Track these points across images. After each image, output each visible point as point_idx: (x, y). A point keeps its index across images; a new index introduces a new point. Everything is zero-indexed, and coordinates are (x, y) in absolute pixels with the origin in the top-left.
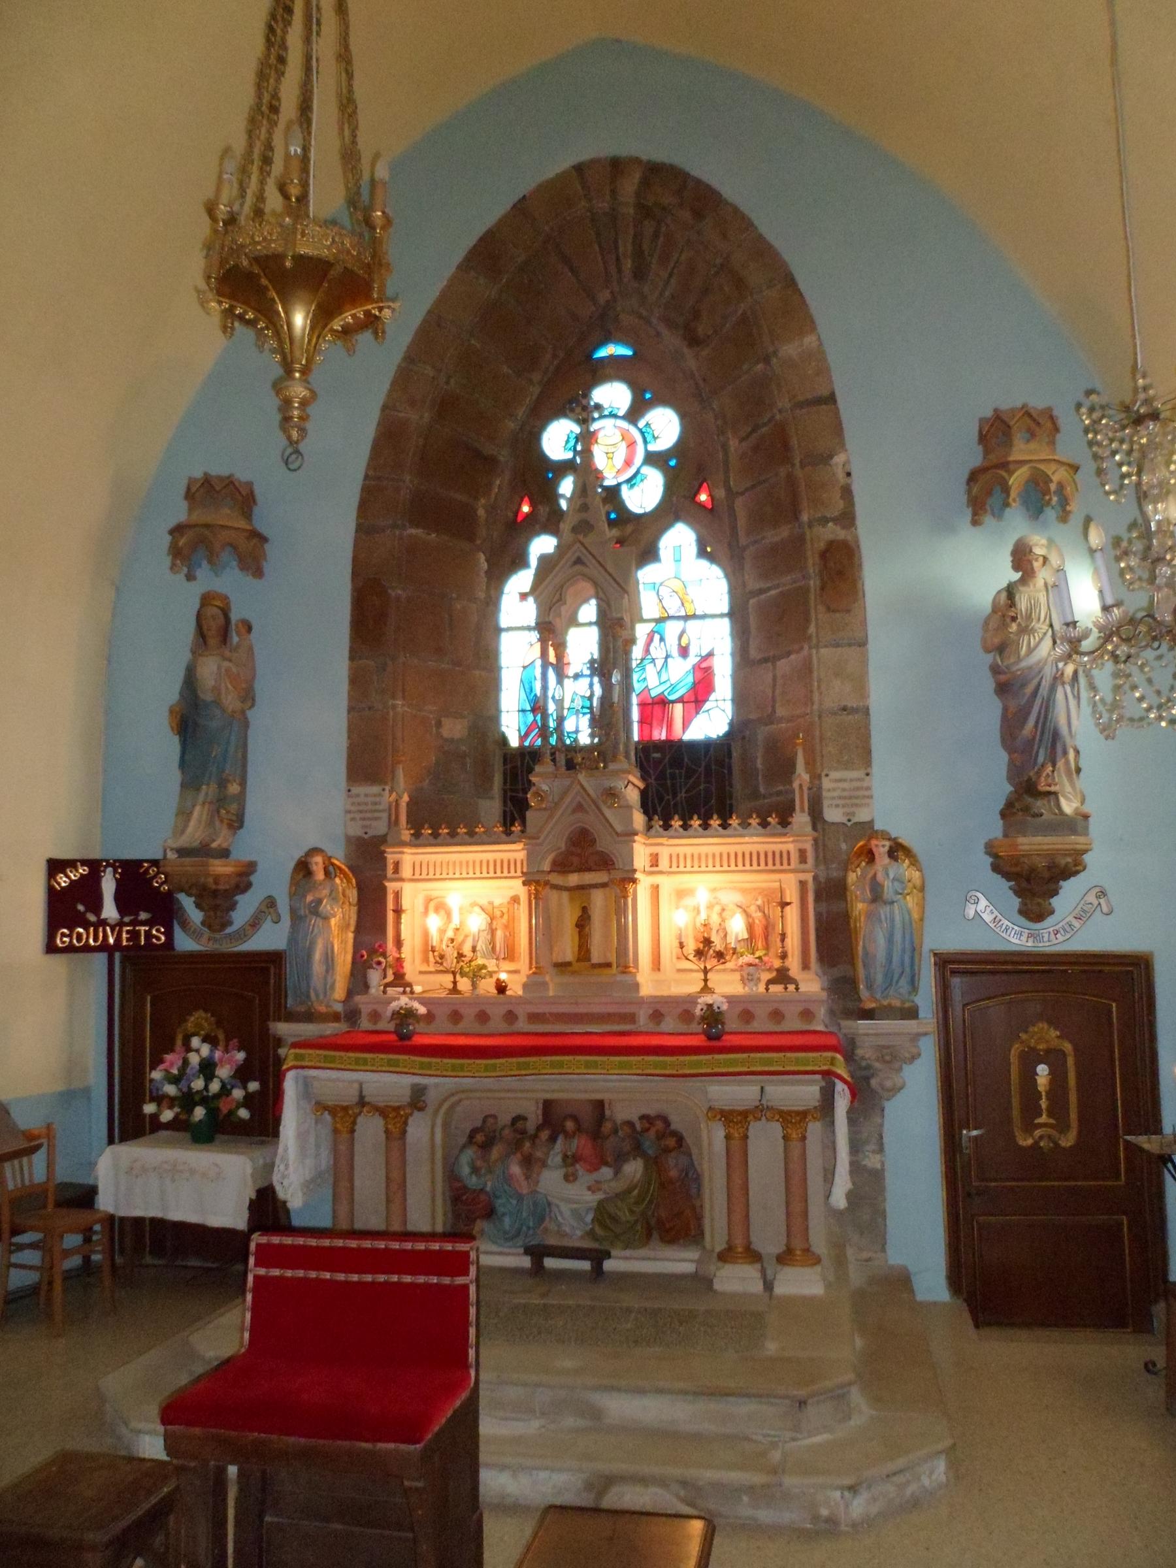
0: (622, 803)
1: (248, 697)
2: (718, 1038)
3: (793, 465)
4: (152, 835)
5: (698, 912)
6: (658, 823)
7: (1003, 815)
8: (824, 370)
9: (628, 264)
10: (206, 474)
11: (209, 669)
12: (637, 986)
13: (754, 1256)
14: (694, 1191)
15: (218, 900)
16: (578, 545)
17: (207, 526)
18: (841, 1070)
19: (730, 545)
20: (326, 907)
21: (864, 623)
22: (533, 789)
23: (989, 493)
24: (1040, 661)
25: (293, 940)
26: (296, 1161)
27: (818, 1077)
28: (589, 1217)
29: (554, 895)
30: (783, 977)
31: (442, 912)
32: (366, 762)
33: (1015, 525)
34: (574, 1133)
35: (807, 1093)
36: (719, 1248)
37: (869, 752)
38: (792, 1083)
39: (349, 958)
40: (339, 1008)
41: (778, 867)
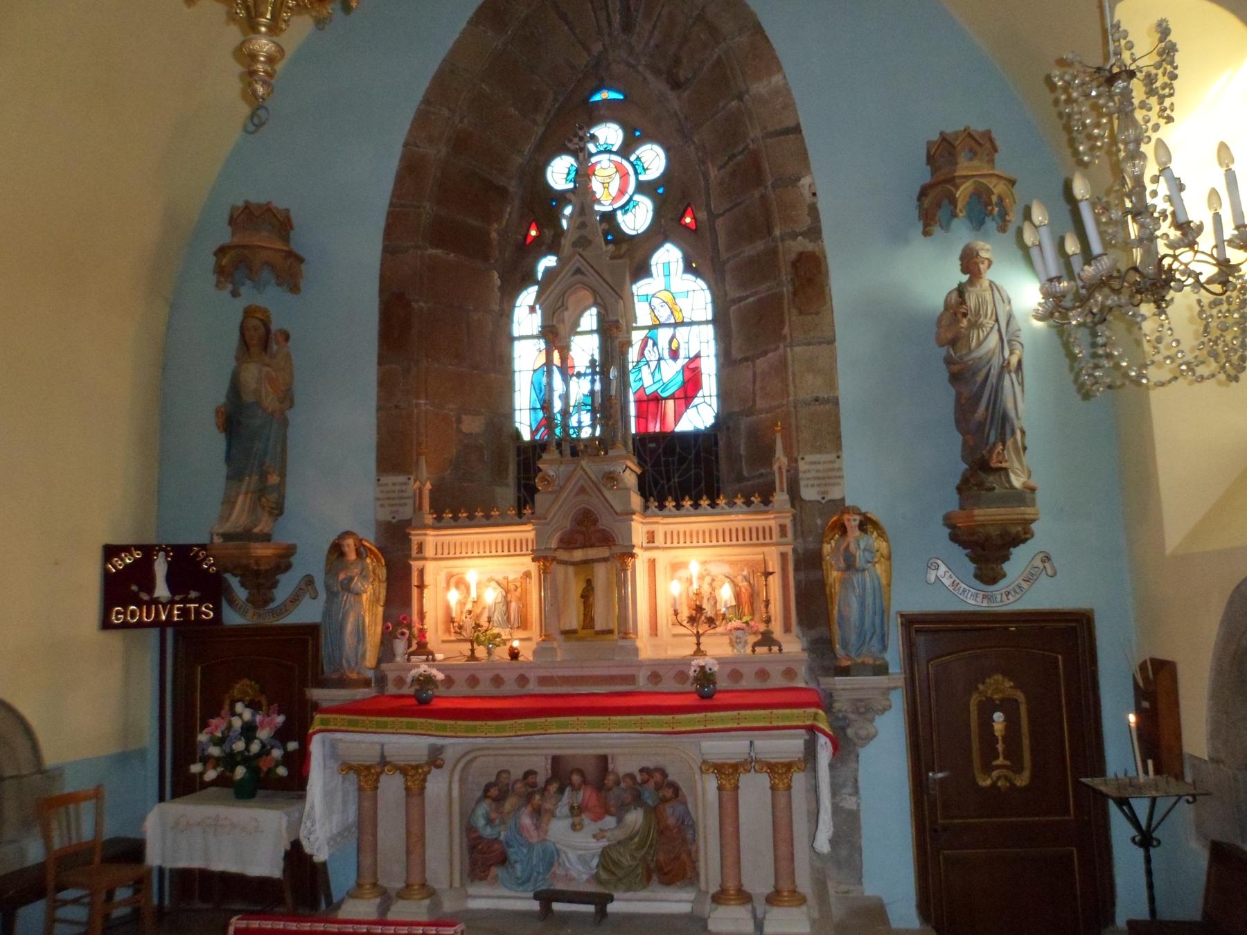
0: (621, 485)
1: (287, 398)
2: (710, 696)
3: (766, 188)
4: (200, 524)
5: (691, 583)
6: (653, 504)
7: (959, 489)
8: (789, 105)
9: (617, 19)
10: (246, 202)
11: (251, 373)
12: (636, 650)
13: (744, 897)
14: (689, 836)
15: (262, 579)
16: (578, 257)
17: (244, 247)
18: (823, 725)
19: (712, 260)
20: (357, 584)
21: (832, 324)
22: (540, 474)
23: (939, 205)
24: (987, 354)
25: (327, 613)
26: (322, 817)
27: (803, 731)
28: (595, 862)
29: (560, 570)
30: (767, 639)
31: (463, 587)
32: (393, 455)
33: (961, 234)
34: (580, 786)
35: (790, 746)
36: (714, 888)
37: (840, 437)
38: (779, 738)
39: (379, 629)
40: (370, 674)
41: (761, 541)
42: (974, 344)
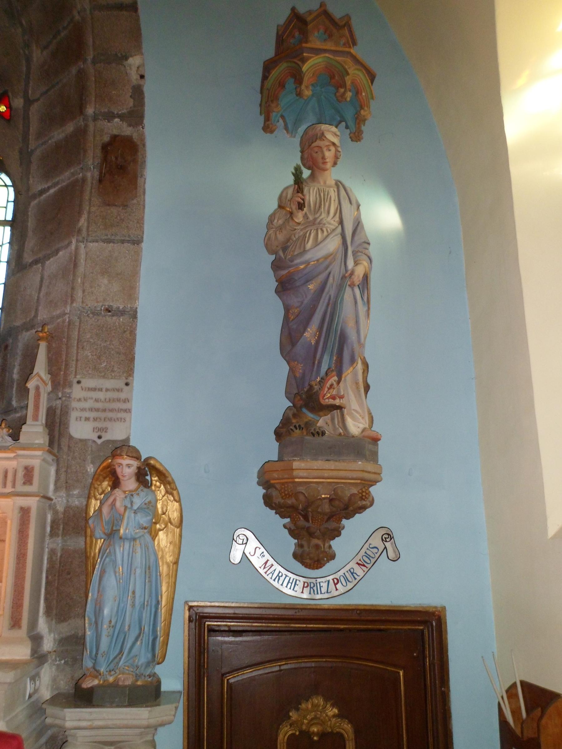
3: (85, 61)
7: (279, 434)
21: (140, 222)
37: (132, 360)
42: (309, 245)
